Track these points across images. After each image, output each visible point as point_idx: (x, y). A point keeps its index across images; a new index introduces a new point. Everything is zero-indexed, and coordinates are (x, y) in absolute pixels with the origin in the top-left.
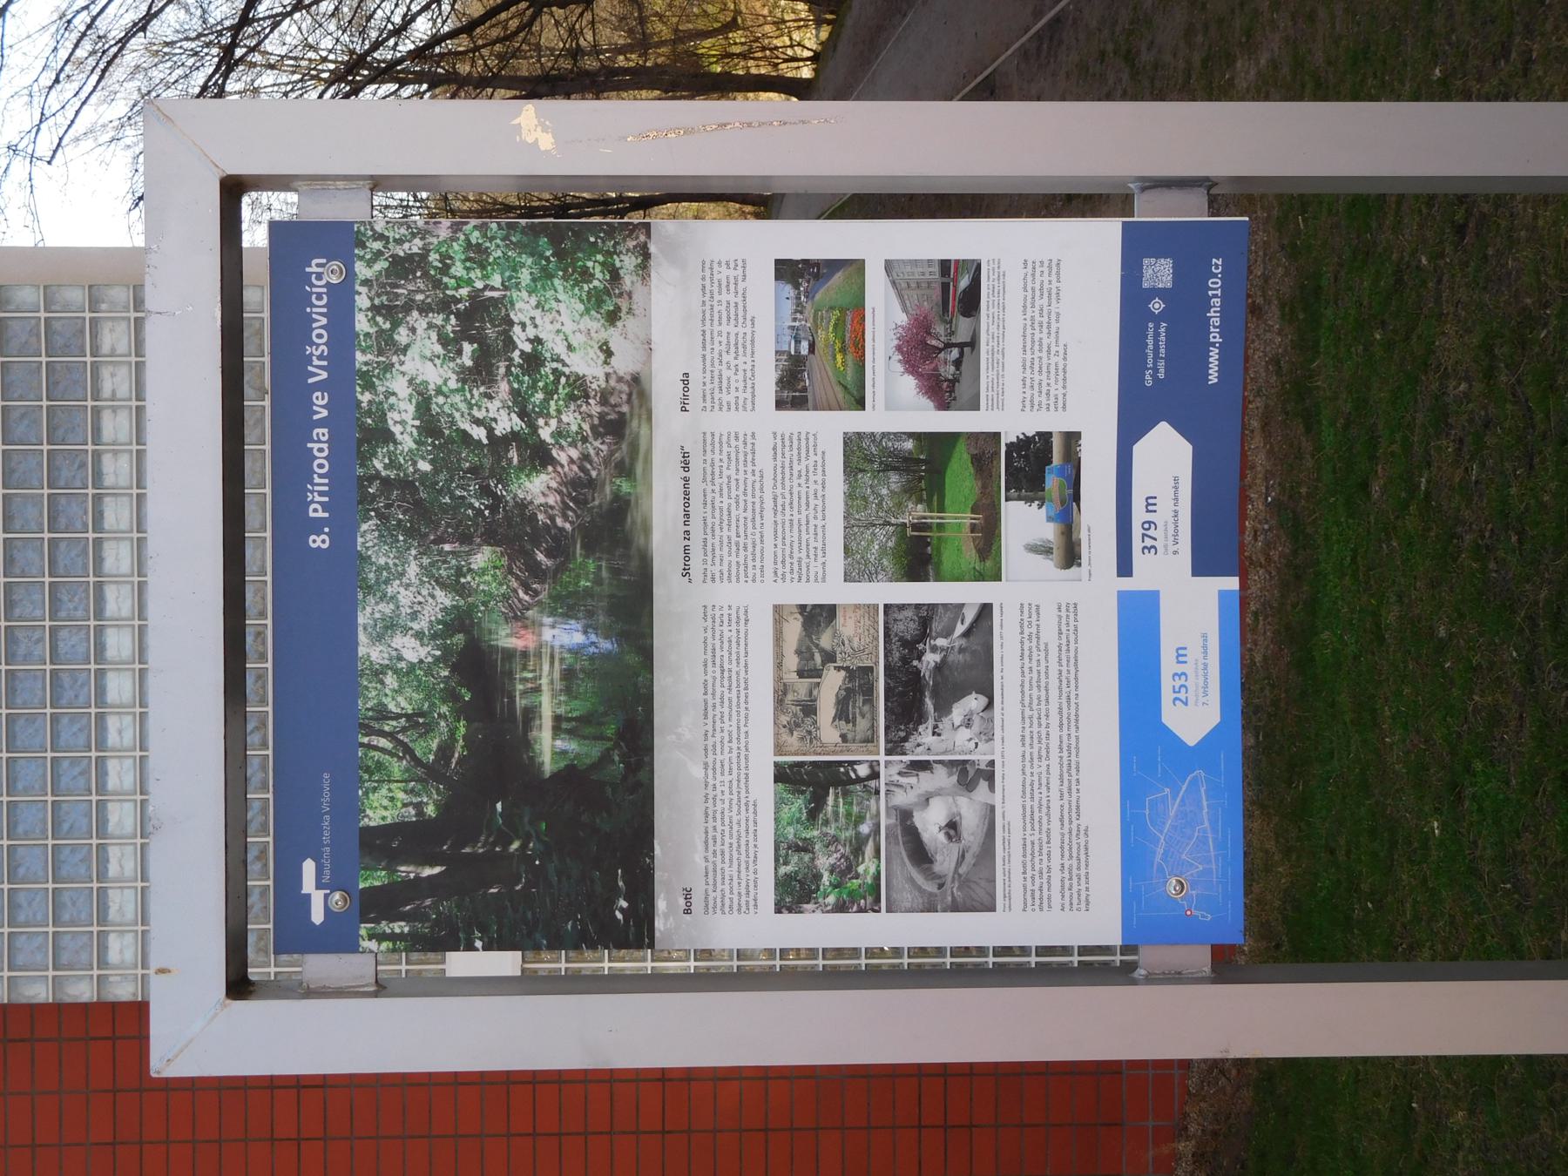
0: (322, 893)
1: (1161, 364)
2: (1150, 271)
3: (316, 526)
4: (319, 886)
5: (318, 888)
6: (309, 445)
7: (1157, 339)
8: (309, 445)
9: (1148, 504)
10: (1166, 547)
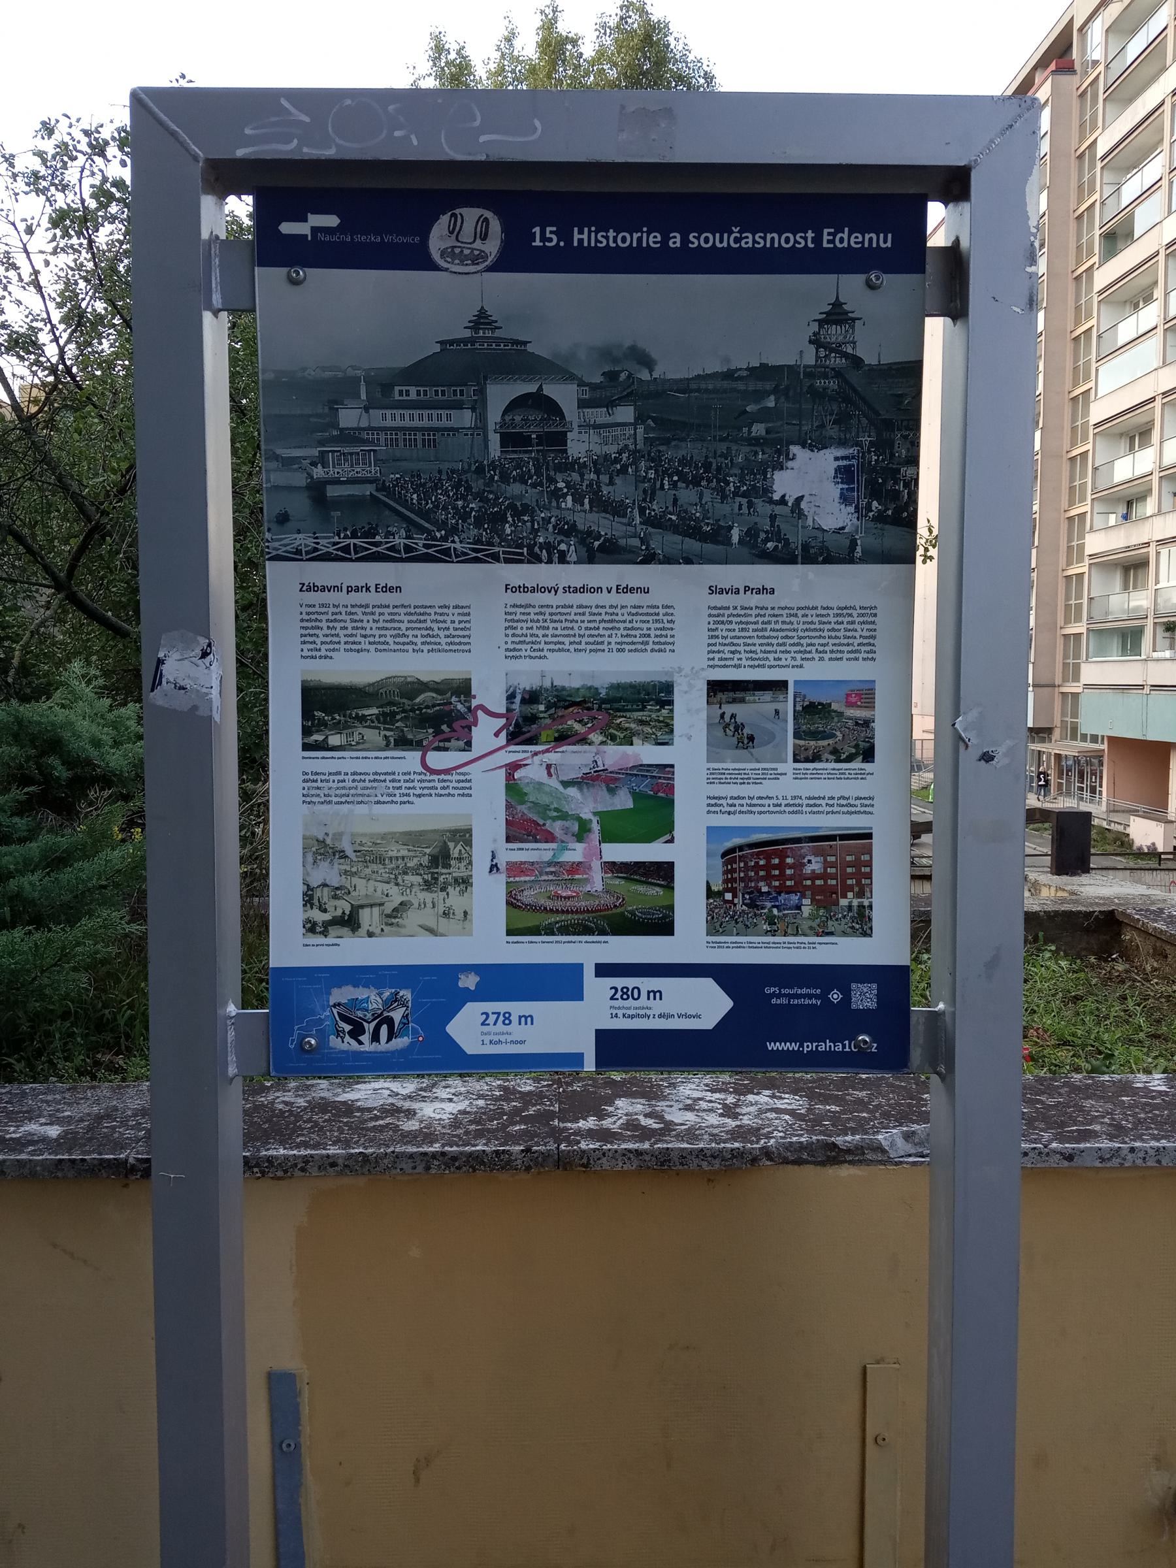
0: (308, 232)
1: (784, 1001)
2: (865, 990)
3: (565, 234)
4: (315, 230)
5: (312, 228)
6: (846, 229)
7: (806, 996)
8: (846, 229)
9: (526, 1018)
10: (489, 1033)
